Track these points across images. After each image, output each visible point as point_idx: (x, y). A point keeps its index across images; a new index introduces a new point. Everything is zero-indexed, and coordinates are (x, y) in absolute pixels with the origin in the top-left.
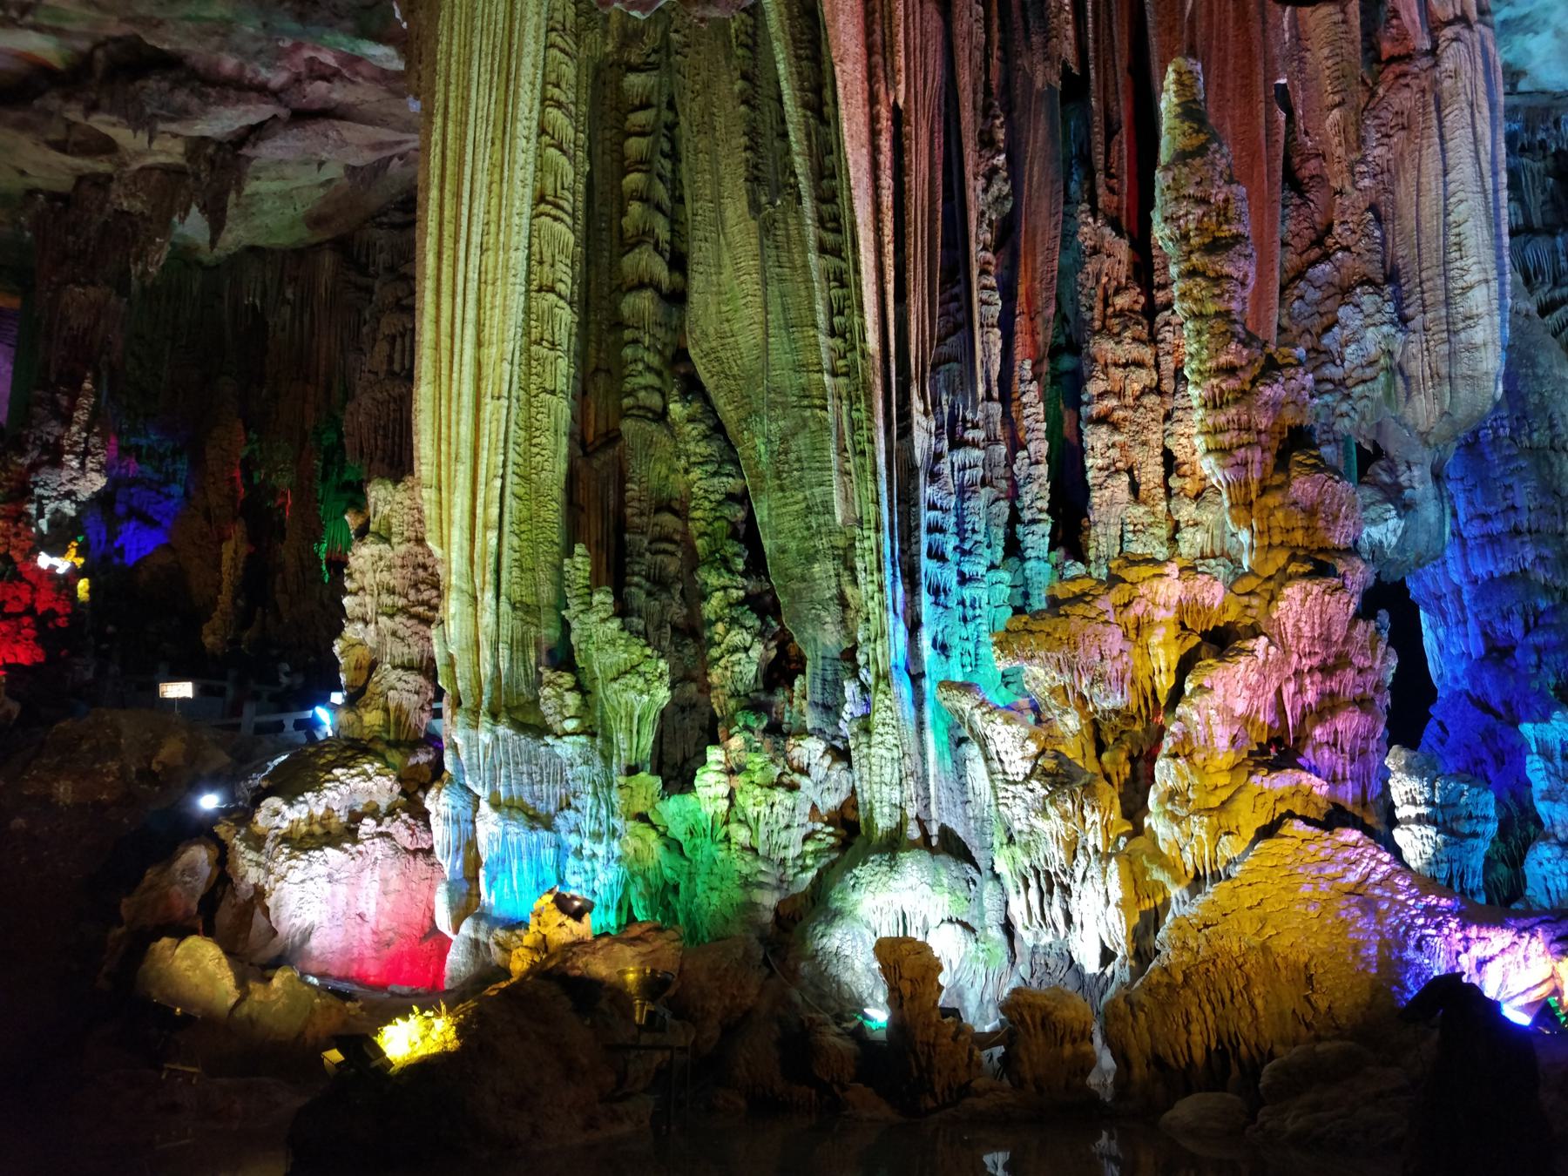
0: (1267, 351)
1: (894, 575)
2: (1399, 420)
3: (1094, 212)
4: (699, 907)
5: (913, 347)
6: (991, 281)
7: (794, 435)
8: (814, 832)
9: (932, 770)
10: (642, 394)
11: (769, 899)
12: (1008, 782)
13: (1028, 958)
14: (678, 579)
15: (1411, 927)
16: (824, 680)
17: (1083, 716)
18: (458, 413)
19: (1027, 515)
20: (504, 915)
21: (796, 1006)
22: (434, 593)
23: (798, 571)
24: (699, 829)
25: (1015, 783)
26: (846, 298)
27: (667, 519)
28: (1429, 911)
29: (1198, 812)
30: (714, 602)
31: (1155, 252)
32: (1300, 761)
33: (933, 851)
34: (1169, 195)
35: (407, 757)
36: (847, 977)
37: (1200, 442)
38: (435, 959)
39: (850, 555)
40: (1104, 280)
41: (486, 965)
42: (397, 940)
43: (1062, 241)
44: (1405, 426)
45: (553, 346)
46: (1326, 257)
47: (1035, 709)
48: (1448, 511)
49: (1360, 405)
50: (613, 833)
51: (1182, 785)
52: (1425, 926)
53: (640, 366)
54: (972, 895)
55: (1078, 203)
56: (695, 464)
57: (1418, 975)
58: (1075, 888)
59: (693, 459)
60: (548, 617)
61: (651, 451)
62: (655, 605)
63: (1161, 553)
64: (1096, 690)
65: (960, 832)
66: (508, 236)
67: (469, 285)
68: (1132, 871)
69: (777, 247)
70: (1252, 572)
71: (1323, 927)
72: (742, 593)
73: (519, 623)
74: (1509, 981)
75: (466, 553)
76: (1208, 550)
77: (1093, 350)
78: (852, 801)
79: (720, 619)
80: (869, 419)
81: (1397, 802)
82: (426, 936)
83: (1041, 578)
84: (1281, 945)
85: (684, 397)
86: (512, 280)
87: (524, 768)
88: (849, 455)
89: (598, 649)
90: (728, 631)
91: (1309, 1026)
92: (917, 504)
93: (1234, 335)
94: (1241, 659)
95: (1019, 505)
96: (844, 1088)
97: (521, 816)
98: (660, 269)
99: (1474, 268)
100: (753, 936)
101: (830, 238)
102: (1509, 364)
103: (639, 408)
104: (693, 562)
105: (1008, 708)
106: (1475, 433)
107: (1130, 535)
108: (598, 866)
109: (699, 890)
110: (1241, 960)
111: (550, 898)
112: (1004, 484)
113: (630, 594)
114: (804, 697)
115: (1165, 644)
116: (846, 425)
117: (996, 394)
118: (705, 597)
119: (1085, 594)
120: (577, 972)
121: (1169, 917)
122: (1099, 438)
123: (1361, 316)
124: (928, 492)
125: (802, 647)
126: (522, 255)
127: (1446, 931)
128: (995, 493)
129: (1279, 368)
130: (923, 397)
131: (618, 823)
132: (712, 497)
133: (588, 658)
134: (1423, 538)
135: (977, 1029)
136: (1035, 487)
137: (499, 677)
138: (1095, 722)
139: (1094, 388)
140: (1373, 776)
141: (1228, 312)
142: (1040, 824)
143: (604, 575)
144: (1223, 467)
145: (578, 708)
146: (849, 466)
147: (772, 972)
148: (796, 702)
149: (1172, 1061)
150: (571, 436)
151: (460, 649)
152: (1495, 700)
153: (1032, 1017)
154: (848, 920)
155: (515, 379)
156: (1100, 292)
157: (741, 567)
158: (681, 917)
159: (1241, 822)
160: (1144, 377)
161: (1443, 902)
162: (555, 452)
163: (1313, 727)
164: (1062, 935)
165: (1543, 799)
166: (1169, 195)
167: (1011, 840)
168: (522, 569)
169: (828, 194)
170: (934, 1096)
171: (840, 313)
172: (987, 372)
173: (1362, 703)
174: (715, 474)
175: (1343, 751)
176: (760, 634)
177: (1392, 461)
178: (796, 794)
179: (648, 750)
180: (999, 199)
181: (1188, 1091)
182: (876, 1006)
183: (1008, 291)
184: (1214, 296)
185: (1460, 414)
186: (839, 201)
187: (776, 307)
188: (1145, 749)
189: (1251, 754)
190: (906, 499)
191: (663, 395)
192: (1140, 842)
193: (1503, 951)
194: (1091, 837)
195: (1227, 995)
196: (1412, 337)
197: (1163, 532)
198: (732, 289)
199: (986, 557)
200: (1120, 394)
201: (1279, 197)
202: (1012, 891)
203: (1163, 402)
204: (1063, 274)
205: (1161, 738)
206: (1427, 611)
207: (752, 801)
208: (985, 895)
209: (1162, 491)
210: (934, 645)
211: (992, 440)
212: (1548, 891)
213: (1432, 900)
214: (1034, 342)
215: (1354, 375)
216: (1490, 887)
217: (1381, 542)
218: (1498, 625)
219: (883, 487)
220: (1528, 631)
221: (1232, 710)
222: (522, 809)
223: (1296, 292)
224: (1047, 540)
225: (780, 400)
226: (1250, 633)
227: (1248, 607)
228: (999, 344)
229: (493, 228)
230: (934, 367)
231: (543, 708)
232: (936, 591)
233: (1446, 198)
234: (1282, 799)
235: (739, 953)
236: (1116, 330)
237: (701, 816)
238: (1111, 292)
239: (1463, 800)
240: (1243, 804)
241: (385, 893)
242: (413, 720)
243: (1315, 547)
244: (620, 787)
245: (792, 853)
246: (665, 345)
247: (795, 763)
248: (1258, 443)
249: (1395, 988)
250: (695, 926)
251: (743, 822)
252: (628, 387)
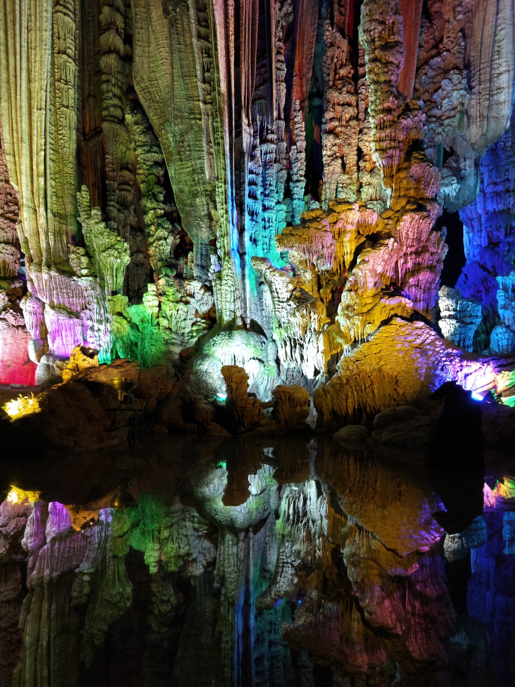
0: (406, 101)
1: (233, 206)
2: (463, 137)
3: (332, 24)
4: (147, 352)
5: (243, 91)
6: (282, 58)
8: (197, 322)
9: (248, 296)
10: (112, 109)
11: (177, 350)
12: (280, 301)
13: (285, 373)
14: (132, 203)
15: (440, 361)
16: (202, 254)
17: (313, 273)
18: (21, 117)
19: (295, 178)
20: (60, 354)
22: (16, 207)
23: (189, 201)
24: (146, 320)
25: (283, 302)
26: (211, 63)
27: (126, 173)
28: (448, 355)
29: (357, 314)
30: (150, 215)
31: (360, 47)
32: (402, 292)
33: (247, 330)
34: (367, 19)
35: (10, 284)
36: (210, 381)
37: (373, 145)
38: (30, 373)
39: (213, 194)
40: (335, 60)
41: (53, 375)
42: (13, 365)
44: (465, 140)
45: (66, 83)
46: (439, 54)
47: (293, 270)
48: (479, 181)
50: (107, 320)
51: (352, 303)
52: (445, 361)
53: (111, 95)
54: (263, 348)
55: (325, 19)
56: (139, 146)
57: (440, 380)
58: (305, 345)
59: (138, 143)
60: (71, 220)
61: (117, 139)
62: (122, 216)
63: (353, 198)
64: (319, 262)
65: (259, 322)
66: (41, 23)
67: (23, 49)
68: (329, 339)
69: (178, 34)
70: (390, 208)
71: (404, 361)
72: (163, 212)
73: (57, 223)
75: (30, 188)
76: (374, 197)
77: (329, 96)
78: (213, 309)
79: (153, 224)
80: (222, 127)
81: (442, 309)
82: (26, 363)
83: (300, 209)
84: (387, 368)
85: (132, 112)
86: (44, 47)
88: (212, 144)
89: (95, 237)
90: (157, 230)
91: (395, 400)
92: (244, 171)
93: (392, 93)
94: (382, 248)
95: (291, 173)
96: (208, 424)
97: (65, 312)
98: (119, 43)
99: (504, 64)
100: (170, 365)
101: (203, 30)
103: (111, 116)
104: (139, 195)
106: (496, 144)
108: (101, 334)
109: (147, 345)
110: (370, 374)
112: (285, 162)
113: (110, 210)
114: (193, 262)
115: (350, 241)
116: (211, 129)
117: (282, 117)
118: (145, 213)
119: (317, 217)
121: (343, 357)
122: (329, 141)
123: (452, 85)
124: (249, 165)
126: (48, 34)
127: (454, 363)
128: (281, 166)
129: (411, 110)
130: (247, 116)
131: (109, 316)
132: (147, 163)
133: (91, 241)
134: (467, 193)
135: (263, 401)
136: (299, 164)
137: (50, 249)
138: (318, 276)
139: (328, 115)
140: (432, 299)
141: (390, 81)
142: (292, 319)
143: (97, 201)
144: (382, 158)
145: (88, 264)
146: (212, 150)
147: (179, 379)
148: (189, 264)
149: (339, 413)
150: (78, 130)
151: (30, 235)
152: (489, 266)
153: (285, 396)
154: (211, 358)
155: (48, 99)
157: (162, 199)
158: (139, 356)
159: (375, 318)
160: (350, 112)
161: (454, 351)
163: (409, 278)
164: (299, 364)
165: (502, 308)
166: (367, 19)
167: (280, 326)
170: (244, 426)
171: (208, 71)
172: (279, 105)
173: (431, 268)
174: (148, 152)
175: (421, 289)
176: (172, 232)
177: (458, 157)
178: (188, 306)
179: (121, 284)
180: (286, 15)
181: (345, 425)
182: (222, 392)
183: (290, 63)
184: (384, 72)
185: (490, 135)
186: (208, 11)
187: (177, 66)
189: (382, 289)
191: (122, 110)
192: (333, 327)
193: (476, 371)
195: (363, 387)
197: (355, 188)
198: (155, 55)
199: (276, 197)
200: (340, 120)
201: (419, 22)
202: (280, 347)
203: (359, 124)
205: (345, 283)
206: (466, 226)
208: (269, 348)
209: (356, 168)
211: (280, 140)
212: (499, 345)
213: (450, 350)
214: (301, 90)
215: (446, 114)
216: (476, 343)
217: (449, 195)
218: (495, 233)
219: (228, 162)
220: (506, 235)
221: (376, 271)
222: (65, 309)
223: (424, 71)
224: (303, 190)
225: (179, 114)
226: (387, 236)
227: (387, 224)
229: (33, 18)
231: (71, 264)
232: (252, 214)
233: (496, 27)
234: (393, 309)
235: (164, 372)
236: (339, 87)
237: (146, 314)
238: (338, 67)
239: (469, 309)
241: (5, 345)
242: (11, 267)
243: (418, 197)
244: (109, 300)
245: (187, 331)
247: (188, 292)
248: (398, 147)
249: (431, 385)
250: (145, 360)
251: (165, 317)
252: (105, 105)
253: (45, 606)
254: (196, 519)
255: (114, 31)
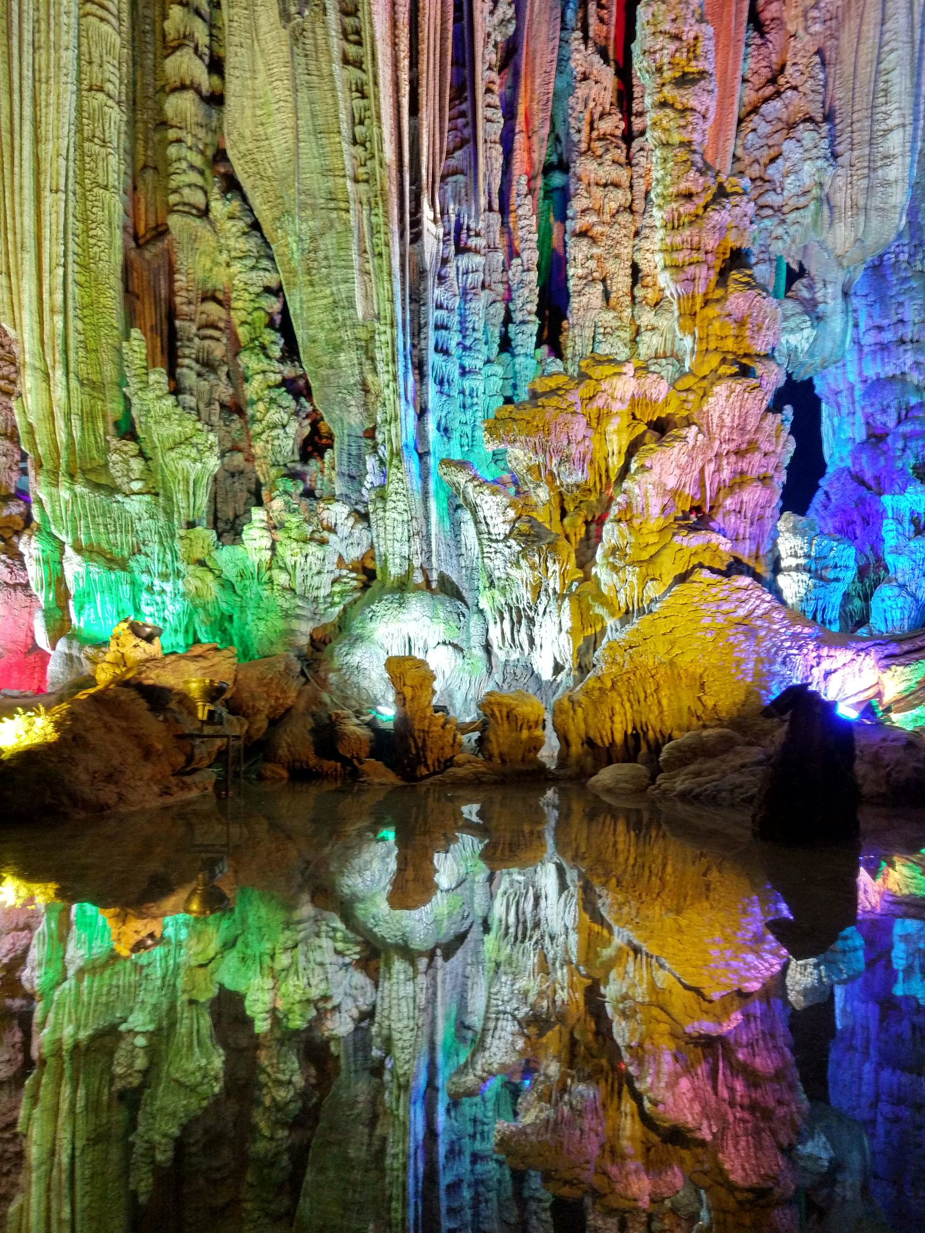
2: (821, 244)
4: (250, 632)
7: (322, 234)
8: (341, 576)
9: (434, 530)
10: (186, 191)
12: (491, 540)
13: (501, 669)
15: (780, 648)
17: (552, 489)
18: (21, 205)
19: (518, 316)
21: (326, 704)
22: (13, 369)
23: (326, 359)
24: (248, 573)
25: (497, 541)
26: (367, 109)
27: (211, 307)
28: (795, 637)
31: (635, 82)
34: (649, 30)
36: (365, 684)
37: (659, 259)
40: (591, 105)
43: (559, 65)
44: (826, 250)
45: (104, 143)
48: (851, 323)
49: (792, 230)
50: (178, 574)
51: (622, 543)
52: (790, 648)
53: (184, 165)
58: (538, 619)
59: (233, 254)
60: (112, 392)
62: (204, 385)
63: (623, 353)
65: (454, 578)
67: (25, 82)
70: (691, 372)
71: (716, 648)
74: (846, 687)
75: (37, 334)
76: (661, 351)
81: (783, 555)
82: (29, 652)
86: (64, 79)
87: (100, 520)
88: (369, 256)
89: (156, 422)
90: (268, 410)
91: (699, 718)
93: (693, 164)
95: (512, 307)
96: (361, 763)
98: (199, 72)
99: (896, 113)
100: (292, 655)
101: (352, 50)
102: (913, 199)
103: (185, 204)
104: (236, 348)
105: (495, 482)
106: (881, 257)
107: (600, 337)
109: (249, 618)
111: (126, 625)
115: (618, 432)
116: (366, 228)
119: (559, 389)
120: (150, 682)
121: (605, 640)
124: (436, 293)
125: (330, 425)
128: (493, 296)
129: (727, 195)
131: (181, 566)
132: (251, 289)
133: (148, 430)
134: (829, 345)
136: (526, 292)
137: (73, 444)
138: (560, 494)
139: (576, 205)
141: (690, 143)
142: (514, 573)
143: (159, 358)
144: (676, 282)
146: (369, 266)
147: (308, 680)
148: (326, 472)
149: (599, 742)
150: (125, 228)
152: (868, 475)
154: (367, 643)
155: (71, 173)
156: (587, 116)
157: (278, 354)
160: (620, 197)
161: (806, 630)
162: (110, 244)
163: (725, 498)
165: (891, 552)
166: (649, 30)
167: (492, 585)
168: (87, 351)
169: (351, 8)
170: (427, 766)
171: (361, 123)
173: (764, 480)
174: (253, 268)
178: (326, 547)
181: (610, 762)
185: (870, 241)
186: (360, 14)
187: (304, 114)
188: (597, 515)
189: (676, 519)
190: (416, 298)
191: (205, 193)
194: (551, 582)
196: (840, 171)
197: (627, 335)
199: (483, 352)
200: (599, 212)
201: (743, 36)
202: (491, 622)
204: (558, 96)
205: (609, 507)
207: (289, 552)
210: (438, 429)
213: (798, 629)
214: (530, 158)
216: (845, 616)
218: (878, 417)
219: (397, 287)
220: (899, 422)
222: (101, 553)
223: (751, 125)
224: (534, 339)
228: (501, 160)
229: (43, 26)
230: (443, 178)
234: (695, 553)
235: (282, 667)
236: (599, 153)
237: (248, 563)
238: (596, 116)
240: (666, 558)
243: (741, 352)
244: (181, 538)
245: (322, 593)
246: (206, 145)
248: (705, 262)
251: (283, 568)
252: (173, 184)
253: (66, 1091)
254: (339, 935)
255: (191, 51)
